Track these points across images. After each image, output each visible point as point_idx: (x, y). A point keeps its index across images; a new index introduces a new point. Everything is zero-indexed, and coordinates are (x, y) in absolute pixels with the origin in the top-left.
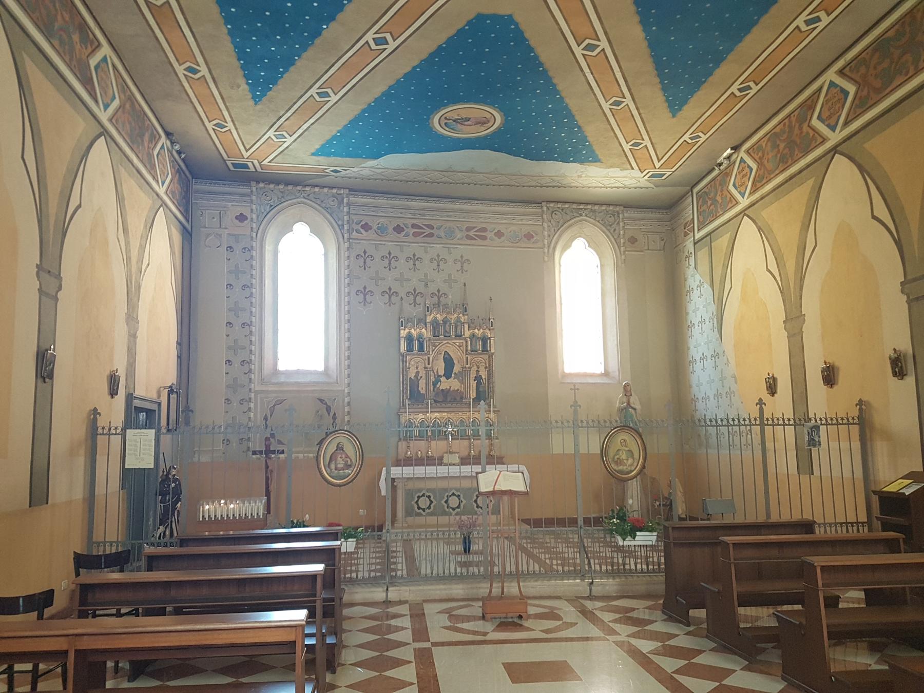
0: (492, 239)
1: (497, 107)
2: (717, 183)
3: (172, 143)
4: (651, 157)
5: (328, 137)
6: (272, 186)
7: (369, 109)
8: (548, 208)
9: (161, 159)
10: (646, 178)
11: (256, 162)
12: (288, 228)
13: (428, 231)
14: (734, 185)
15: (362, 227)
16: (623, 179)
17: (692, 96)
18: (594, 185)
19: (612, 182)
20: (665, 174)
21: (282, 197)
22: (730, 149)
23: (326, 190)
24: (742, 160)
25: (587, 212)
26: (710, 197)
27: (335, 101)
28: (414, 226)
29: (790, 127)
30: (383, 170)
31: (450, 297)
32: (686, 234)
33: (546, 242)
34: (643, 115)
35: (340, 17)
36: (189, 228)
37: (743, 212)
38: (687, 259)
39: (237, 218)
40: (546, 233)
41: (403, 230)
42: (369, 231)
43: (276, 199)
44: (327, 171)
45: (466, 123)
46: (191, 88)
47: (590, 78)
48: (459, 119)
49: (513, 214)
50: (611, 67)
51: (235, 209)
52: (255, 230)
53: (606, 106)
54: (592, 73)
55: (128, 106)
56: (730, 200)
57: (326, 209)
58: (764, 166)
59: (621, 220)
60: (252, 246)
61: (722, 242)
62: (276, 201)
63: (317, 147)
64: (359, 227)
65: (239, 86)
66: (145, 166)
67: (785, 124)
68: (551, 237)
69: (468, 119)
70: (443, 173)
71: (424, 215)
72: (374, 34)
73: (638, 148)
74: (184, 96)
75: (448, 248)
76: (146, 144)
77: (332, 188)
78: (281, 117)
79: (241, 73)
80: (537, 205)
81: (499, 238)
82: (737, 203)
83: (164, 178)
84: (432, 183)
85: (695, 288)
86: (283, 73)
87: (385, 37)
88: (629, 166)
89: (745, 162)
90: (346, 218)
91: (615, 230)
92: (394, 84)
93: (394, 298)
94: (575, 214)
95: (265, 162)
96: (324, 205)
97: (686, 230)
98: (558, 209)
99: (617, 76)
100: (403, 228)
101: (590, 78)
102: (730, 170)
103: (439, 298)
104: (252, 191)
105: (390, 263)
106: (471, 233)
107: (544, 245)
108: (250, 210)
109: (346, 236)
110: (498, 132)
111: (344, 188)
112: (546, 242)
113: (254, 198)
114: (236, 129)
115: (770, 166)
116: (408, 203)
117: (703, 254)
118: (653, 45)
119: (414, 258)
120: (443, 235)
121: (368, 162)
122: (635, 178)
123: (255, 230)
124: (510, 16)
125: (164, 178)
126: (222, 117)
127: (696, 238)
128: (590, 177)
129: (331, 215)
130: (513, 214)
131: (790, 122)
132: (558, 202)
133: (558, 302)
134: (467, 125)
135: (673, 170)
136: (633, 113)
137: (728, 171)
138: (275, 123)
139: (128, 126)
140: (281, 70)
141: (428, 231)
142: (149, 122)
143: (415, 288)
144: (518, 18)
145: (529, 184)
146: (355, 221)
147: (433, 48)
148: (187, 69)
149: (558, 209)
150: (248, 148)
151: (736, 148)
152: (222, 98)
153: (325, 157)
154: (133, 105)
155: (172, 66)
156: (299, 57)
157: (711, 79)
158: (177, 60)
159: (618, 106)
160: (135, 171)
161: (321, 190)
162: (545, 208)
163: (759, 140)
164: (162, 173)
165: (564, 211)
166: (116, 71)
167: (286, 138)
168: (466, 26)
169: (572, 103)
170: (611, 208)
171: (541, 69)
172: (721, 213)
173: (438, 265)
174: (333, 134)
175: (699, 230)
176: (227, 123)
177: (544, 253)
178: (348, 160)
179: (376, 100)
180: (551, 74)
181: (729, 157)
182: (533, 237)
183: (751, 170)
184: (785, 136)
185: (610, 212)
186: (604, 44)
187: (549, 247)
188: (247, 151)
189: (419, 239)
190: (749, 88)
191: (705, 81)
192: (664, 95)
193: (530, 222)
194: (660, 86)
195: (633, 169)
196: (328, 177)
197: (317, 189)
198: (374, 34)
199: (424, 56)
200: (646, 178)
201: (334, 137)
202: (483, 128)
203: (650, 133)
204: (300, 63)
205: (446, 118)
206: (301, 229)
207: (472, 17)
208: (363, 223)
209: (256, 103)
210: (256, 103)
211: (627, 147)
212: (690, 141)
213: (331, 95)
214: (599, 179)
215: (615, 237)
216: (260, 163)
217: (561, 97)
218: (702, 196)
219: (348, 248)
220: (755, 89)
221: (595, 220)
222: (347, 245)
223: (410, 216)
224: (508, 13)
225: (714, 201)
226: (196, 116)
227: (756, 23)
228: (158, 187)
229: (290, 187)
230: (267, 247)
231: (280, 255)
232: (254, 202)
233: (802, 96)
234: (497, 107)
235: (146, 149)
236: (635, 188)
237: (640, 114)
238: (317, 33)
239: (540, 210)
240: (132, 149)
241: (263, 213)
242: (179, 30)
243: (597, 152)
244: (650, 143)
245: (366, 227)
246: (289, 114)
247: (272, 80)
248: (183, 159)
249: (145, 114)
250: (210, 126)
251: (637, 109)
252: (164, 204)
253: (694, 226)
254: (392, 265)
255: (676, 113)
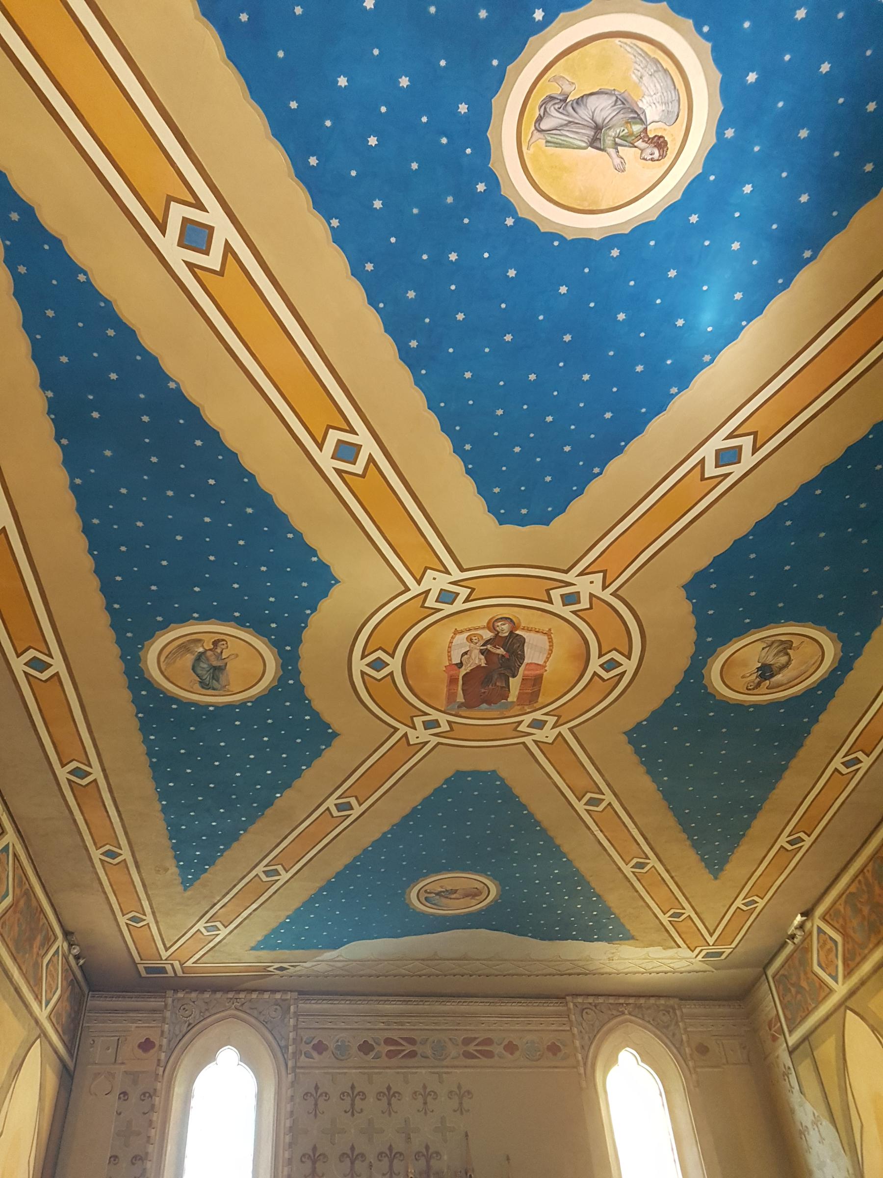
0: (501, 1057)
1: (489, 875)
2: (797, 962)
3: (70, 945)
4: (698, 930)
5: (274, 925)
6: (194, 995)
7: (329, 887)
8: (575, 1005)
9: (52, 969)
10: (700, 957)
11: (177, 964)
12: (209, 1056)
13: (409, 1048)
14: (820, 965)
15: (315, 1047)
16: (671, 961)
17: (733, 853)
18: (630, 970)
19: (655, 965)
20: (724, 952)
21: (207, 1010)
22: (799, 915)
23: (266, 995)
24: (820, 930)
25: (630, 1008)
26: (792, 982)
27: (286, 879)
28: (388, 1041)
29: (868, 884)
30: (346, 963)
31: (445, 1157)
32: (775, 1039)
33: (580, 1057)
34: (676, 879)
35: (297, 783)
36: (71, 1065)
37: (843, 1005)
38: (786, 1078)
39: (140, 1046)
40: (577, 1043)
41: (372, 1048)
42: (324, 1053)
43: (198, 1012)
44: (269, 969)
45: (453, 896)
46: (107, 874)
47: (600, 836)
48: (443, 892)
49: (526, 1015)
50: (624, 823)
51: (138, 1031)
52: (163, 1064)
53: (627, 870)
54: (601, 831)
55: (22, 902)
56: (821, 987)
57: (264, 1023)
58: (851, 937)
59: (679, 1019)
60: (155, 1090)
61: (827, 1050)
62: (197, 1018)
63: (260, 938)
64: (308, 1048)
65: (166, 870)
66: (28, 982)
67: (860, 882)
68: (586, 1048)
69: (455, 891)
70: (426, 962)
71: (402, 1024)
72: (337, 799)
73: (680, 919)
74: (96, 885)
75: (437, 1073)
76: (35, 950)
77: (274, 991)
78: (215, 904)
79: (171, 853)
80: (560, 1001)
81: (512, 1054)
82: (831, 991)
83: (50, 995)
84: (413, 976)
85: (810, 1126)
86: (222, 851)
87: (339, 811)
88: (673, 944)
89: (825, 933)
90: (291, 1035)
91: (674, 1035)
92: (361, 855)
93: (358, 1164)
94: (615, 1013)
95: (188, 964)
96: (262, 1018)
97: (772, 1032)
98: (589, 1006)
99: (634, 834)
100: (372, 1045)
101: (600, 836)
102: (808, 943)
103: (428, 1162)
104: (166, 1005)
105: (353, 1105)
106: (471, 1048)
107: (578, 1061)
108: (160, 1032)
109: (290, 1064)
110: (495, 904)
111: (291, 991)
112: (580, 1057)
113: (168, 1014)
114: (157, 922)
115: (858, 937)
116: (380, 1007)
117: (805, 1068)
118: (669, 796)
119: (389, 1092)
120: (429, 1052)
121: (325, 954)
122: (684, 958)
123: (163, 1064)
124: (494, 772)
125: (50, 995)
126: (141, 910)
127: (790, 1044)
128: (626, 959)
129: (270, 1032)
130: (526, 1015)
131: (866, 879)
132: (588, 995)
133: (612, 1159)
134: (454, 899)
135: (733, 946)
136: (663, 876)
137: (805, 945)
138: (207, 912)
139: (16, 928)
140: (222, 847)
141: (409, 1048)
142: (46, 921)
143: (391, 1146)
144: (503, 774)
145: (544, 972)
146: (304, 1040)
147: (408, 810)
148: (105, 854)
149: (589, 1006)
150: (168, 946)
151: (807, 914)
152: (144, 886)
153: (269, 951)
154: (29, 900)
155: (87, 850)
156: (245, 831)
157: (750, 832)
158: (95, 844)
159: (643, 868)
160: (12, 990)
161: (260, 996)
162: (571, 1005)
163: (834, 903)
164: (49, 986)
165: (598, 1007)
166: (16, 861)
167: (219, 930)
168: (443, 784)
169: (583, 866)
170: (662, 1001)
171: (538, 828)
172: (813, 1005)
173: (425, 1103)
174: (281, 920)
175: (790, 1032)
176: (145, 915)
177: (580, 1074)
178: (299, 953)
179: (338, 875)
180: (551, 834)
181: (801, 926)
182: (559, 1050)
183: (835, 942)
184: (865, 896)
185: (662, 1008)
186: (609, 797)
187: (585, 1064)
188: (167, 949)
189: (394, 1061)
190: (858, 761)
191: (744, 835)
192: (697, 853)
193: (553, 1027)
194: (688, 843)
195: (679, 947)
196: (272, 977)
197: (254, 996)
198: (337, 799)
199: (396, 820)
200: (700, 957)
201: (282, 925)
202: (474, 902)
203: (690, 900)
204: (246, 838)
205: (426, 891)
206: (228, 1056)
207: (450, 775)
208: (315, 1042)
209: (186, 889)
210: (186, 889)
211: (665, 919)
212: (789, 847)
213: (281, 872)
214: (638, 962)
215: (676, 1045)
216: (181, 965)
217: (568, 860)
218: (781, 979)
219: (293, 1083)
220: (808, 841)
221: (643, 1019)
222: (291, 1077)
223: (382, 1026)
224: (492, 768)
225: (800, 990)
226: (107, 907)
227: (785, 768)
228: (39, 1010)
229: (218, 995)
230: (176, 1089)
231: (194, 1103)
232: (167, 1021)
233: (860, 858)
234: (489, 875)
235: (35, 956)
236: (689, 972)
237: (672, 877)
238: (270, 803)
239: (565, 1008)
240: (15, 959)
241: (177, 1036)
242: (103, 808)
243: (628, 927)
244: (693, 912)
245: (320, 1048)
246: (226, 900)
247: (209, 860)
248: (81, 966)
249: (42, 911)
250: (122, 920)
251: (668, 871)
252: (44, 1034)
253: (781, 1025)
254: (356, 1106)
255: (718, 875)
